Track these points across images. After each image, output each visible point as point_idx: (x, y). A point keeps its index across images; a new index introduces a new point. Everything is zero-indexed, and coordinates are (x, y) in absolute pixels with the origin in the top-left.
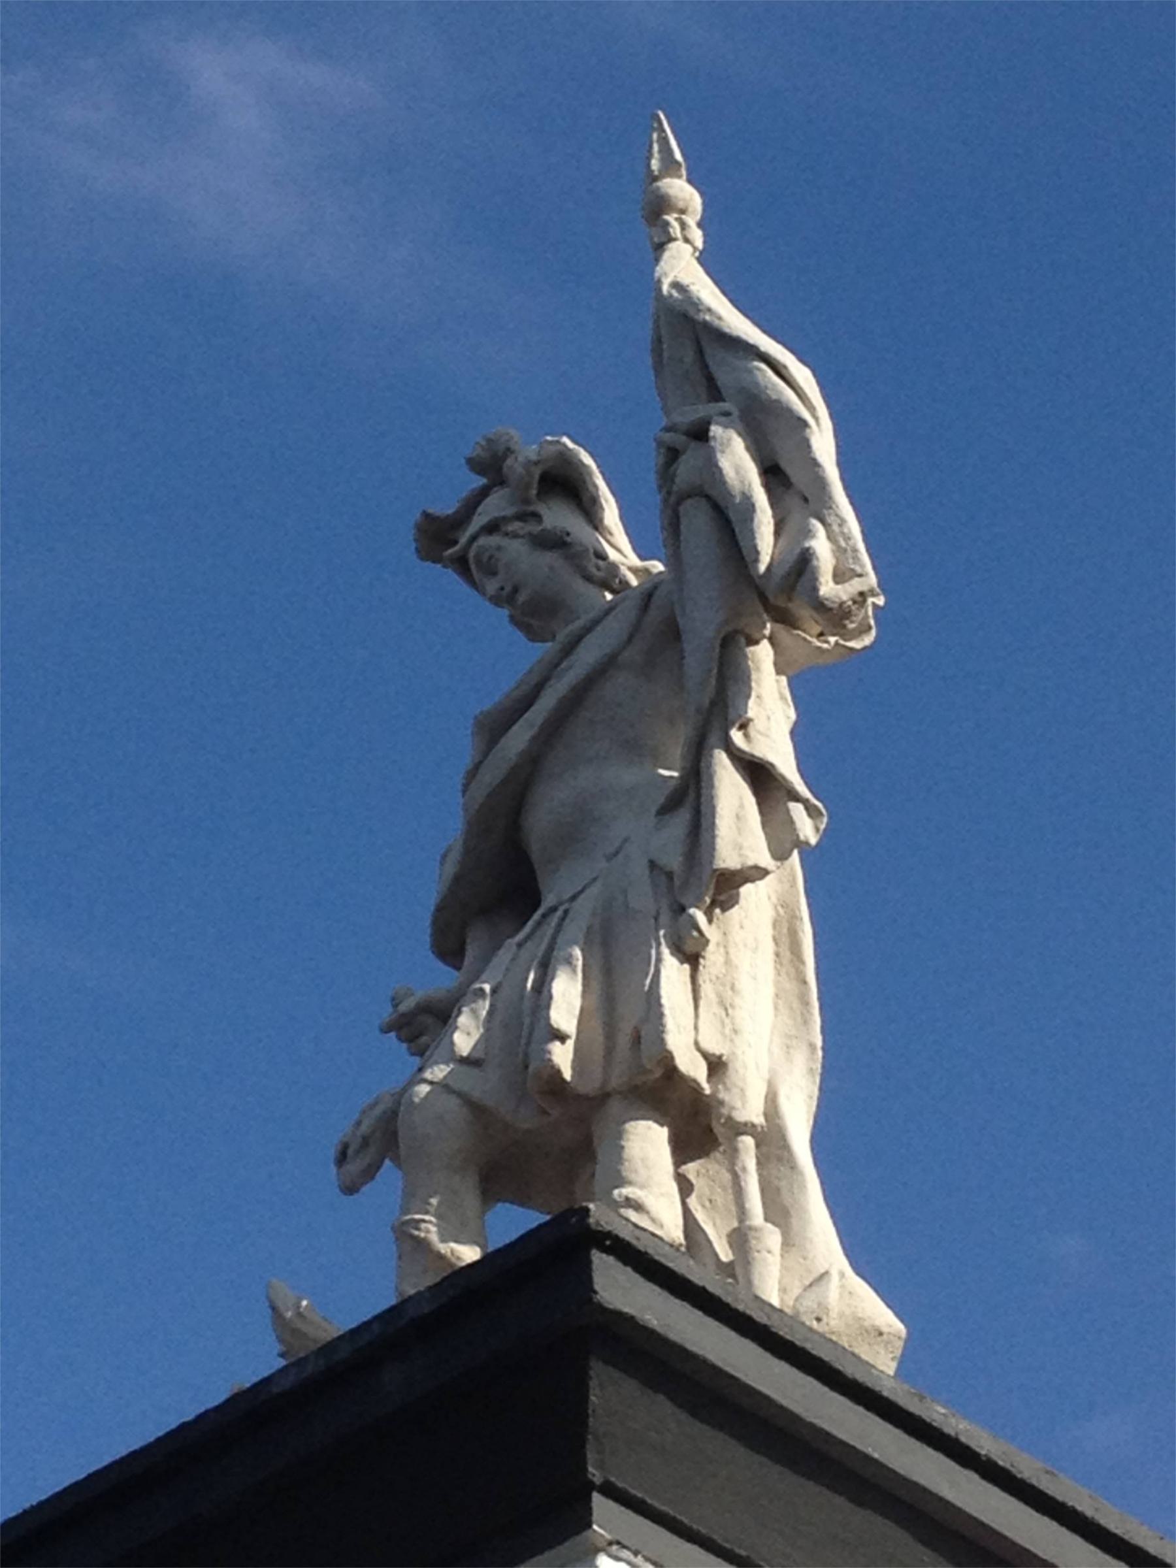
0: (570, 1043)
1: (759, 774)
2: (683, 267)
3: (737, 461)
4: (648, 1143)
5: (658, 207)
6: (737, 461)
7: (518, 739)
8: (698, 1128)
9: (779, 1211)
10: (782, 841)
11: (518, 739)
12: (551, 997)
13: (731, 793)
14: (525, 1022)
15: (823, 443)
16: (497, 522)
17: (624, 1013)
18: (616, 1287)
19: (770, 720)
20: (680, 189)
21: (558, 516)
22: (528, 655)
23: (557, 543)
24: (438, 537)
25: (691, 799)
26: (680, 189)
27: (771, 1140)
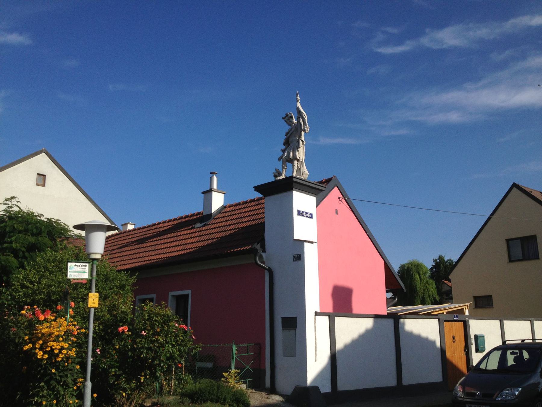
0: (315, 245)
1: (302, 141)
2: (299, 105)
3: (301, 121)
4: (296, 162)
5: (297, 99)
6: (301, 121)
7: (288, 135)
8: (298, 160)
9: (303, 166)
10: (303, 144)
11: (288, 135)
12: (411, 263)
13: (301, 142)
14: (289, 154)
15: (306, 120)
16: (288, 119)
17: (294, 155)
18: (294, 180)
19: (303, 138)
20: (298, 98)
21: (291, 120)
22: (290, 127)
23: (291, 121)
24: (283, 118)
25: (298, 142)
26: (298, 98)
27: (302, 161)
